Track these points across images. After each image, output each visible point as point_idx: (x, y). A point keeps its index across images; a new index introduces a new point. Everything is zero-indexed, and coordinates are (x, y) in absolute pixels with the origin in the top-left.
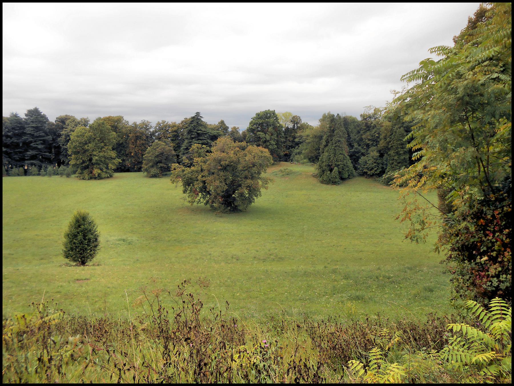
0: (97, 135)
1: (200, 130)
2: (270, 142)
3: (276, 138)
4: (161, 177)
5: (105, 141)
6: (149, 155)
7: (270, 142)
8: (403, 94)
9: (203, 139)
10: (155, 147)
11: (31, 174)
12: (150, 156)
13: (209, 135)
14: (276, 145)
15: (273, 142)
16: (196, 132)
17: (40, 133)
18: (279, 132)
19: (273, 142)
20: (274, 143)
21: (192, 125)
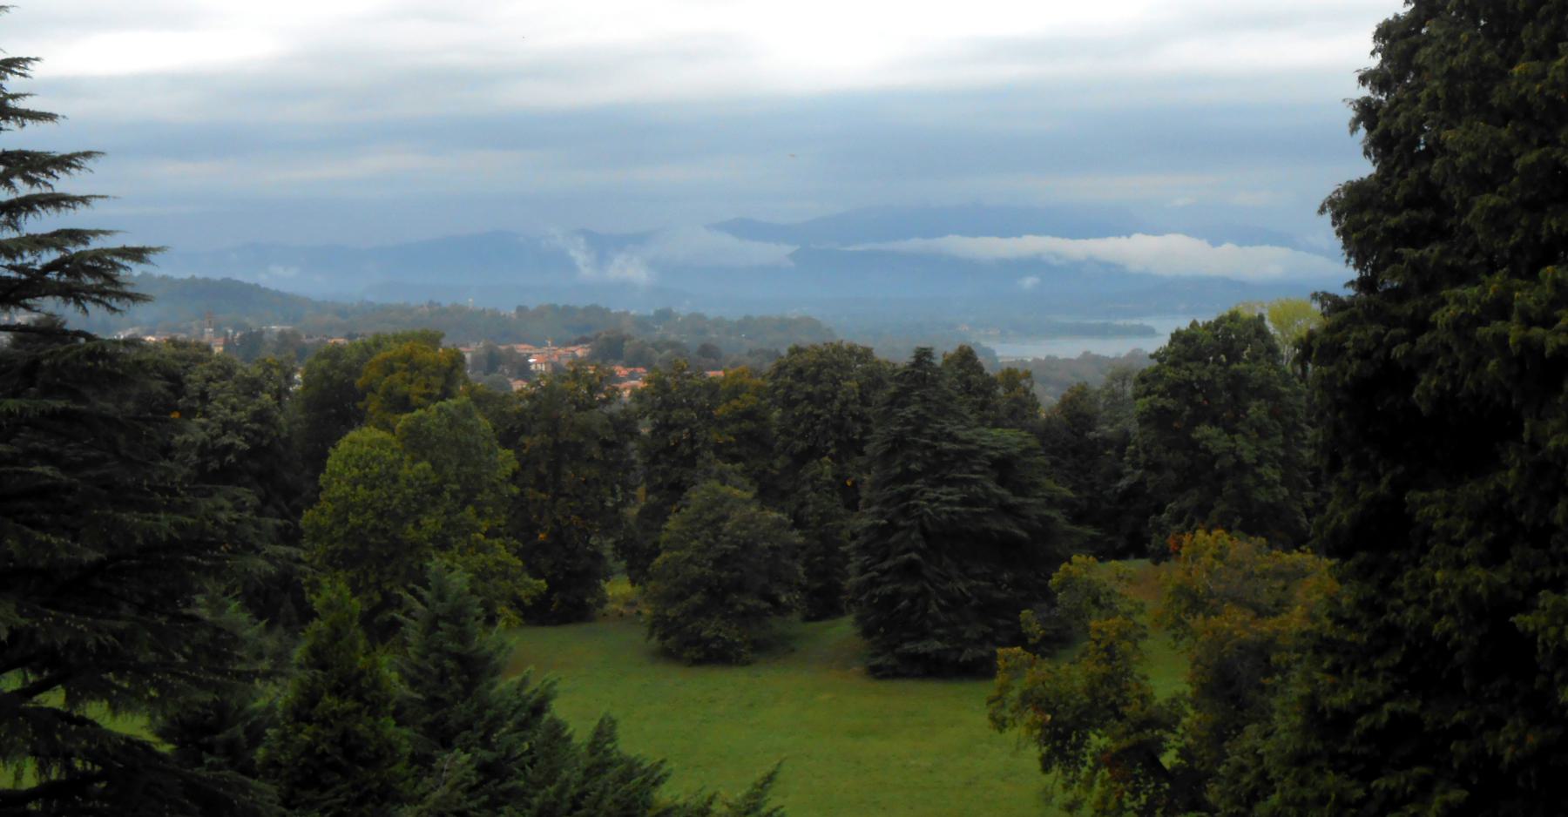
0: (450, 471)
1: (952, 438)
2: (1258, 470)
3: (1281, 453)
4: (748, 663)
5: (479, 497)
6: (686, 554)
7: (1258, 470)
8: (1494, 284)
9: (964, 480)
10: (710, 516)
11: (1334, 193)
12: (690, 560)
13: (989, 457)
14: (1283, 484)
15: (1270, 473)
16: (927, 446)
17: (1448, 310)
18: (1290, 419)
19: (1270, 473)
20: (1277, 477)
21: (908, 412)
